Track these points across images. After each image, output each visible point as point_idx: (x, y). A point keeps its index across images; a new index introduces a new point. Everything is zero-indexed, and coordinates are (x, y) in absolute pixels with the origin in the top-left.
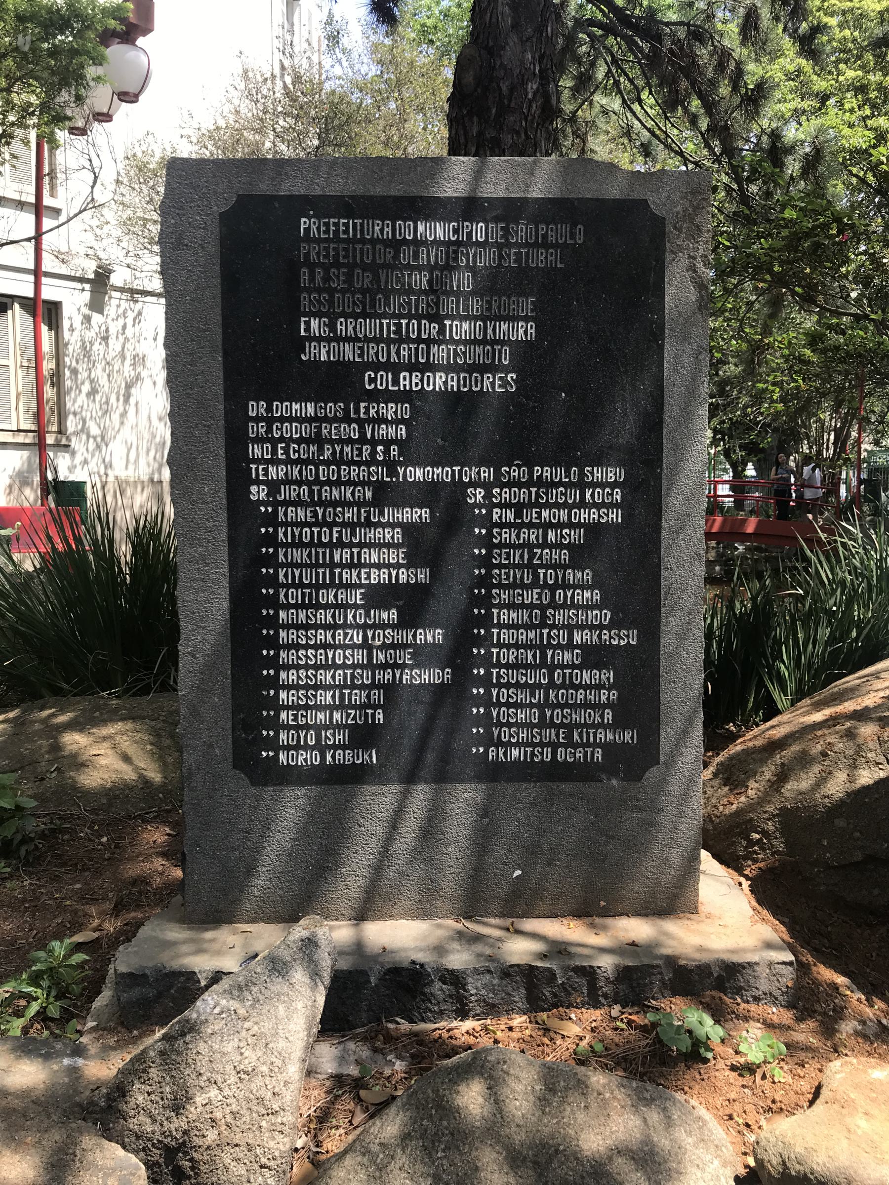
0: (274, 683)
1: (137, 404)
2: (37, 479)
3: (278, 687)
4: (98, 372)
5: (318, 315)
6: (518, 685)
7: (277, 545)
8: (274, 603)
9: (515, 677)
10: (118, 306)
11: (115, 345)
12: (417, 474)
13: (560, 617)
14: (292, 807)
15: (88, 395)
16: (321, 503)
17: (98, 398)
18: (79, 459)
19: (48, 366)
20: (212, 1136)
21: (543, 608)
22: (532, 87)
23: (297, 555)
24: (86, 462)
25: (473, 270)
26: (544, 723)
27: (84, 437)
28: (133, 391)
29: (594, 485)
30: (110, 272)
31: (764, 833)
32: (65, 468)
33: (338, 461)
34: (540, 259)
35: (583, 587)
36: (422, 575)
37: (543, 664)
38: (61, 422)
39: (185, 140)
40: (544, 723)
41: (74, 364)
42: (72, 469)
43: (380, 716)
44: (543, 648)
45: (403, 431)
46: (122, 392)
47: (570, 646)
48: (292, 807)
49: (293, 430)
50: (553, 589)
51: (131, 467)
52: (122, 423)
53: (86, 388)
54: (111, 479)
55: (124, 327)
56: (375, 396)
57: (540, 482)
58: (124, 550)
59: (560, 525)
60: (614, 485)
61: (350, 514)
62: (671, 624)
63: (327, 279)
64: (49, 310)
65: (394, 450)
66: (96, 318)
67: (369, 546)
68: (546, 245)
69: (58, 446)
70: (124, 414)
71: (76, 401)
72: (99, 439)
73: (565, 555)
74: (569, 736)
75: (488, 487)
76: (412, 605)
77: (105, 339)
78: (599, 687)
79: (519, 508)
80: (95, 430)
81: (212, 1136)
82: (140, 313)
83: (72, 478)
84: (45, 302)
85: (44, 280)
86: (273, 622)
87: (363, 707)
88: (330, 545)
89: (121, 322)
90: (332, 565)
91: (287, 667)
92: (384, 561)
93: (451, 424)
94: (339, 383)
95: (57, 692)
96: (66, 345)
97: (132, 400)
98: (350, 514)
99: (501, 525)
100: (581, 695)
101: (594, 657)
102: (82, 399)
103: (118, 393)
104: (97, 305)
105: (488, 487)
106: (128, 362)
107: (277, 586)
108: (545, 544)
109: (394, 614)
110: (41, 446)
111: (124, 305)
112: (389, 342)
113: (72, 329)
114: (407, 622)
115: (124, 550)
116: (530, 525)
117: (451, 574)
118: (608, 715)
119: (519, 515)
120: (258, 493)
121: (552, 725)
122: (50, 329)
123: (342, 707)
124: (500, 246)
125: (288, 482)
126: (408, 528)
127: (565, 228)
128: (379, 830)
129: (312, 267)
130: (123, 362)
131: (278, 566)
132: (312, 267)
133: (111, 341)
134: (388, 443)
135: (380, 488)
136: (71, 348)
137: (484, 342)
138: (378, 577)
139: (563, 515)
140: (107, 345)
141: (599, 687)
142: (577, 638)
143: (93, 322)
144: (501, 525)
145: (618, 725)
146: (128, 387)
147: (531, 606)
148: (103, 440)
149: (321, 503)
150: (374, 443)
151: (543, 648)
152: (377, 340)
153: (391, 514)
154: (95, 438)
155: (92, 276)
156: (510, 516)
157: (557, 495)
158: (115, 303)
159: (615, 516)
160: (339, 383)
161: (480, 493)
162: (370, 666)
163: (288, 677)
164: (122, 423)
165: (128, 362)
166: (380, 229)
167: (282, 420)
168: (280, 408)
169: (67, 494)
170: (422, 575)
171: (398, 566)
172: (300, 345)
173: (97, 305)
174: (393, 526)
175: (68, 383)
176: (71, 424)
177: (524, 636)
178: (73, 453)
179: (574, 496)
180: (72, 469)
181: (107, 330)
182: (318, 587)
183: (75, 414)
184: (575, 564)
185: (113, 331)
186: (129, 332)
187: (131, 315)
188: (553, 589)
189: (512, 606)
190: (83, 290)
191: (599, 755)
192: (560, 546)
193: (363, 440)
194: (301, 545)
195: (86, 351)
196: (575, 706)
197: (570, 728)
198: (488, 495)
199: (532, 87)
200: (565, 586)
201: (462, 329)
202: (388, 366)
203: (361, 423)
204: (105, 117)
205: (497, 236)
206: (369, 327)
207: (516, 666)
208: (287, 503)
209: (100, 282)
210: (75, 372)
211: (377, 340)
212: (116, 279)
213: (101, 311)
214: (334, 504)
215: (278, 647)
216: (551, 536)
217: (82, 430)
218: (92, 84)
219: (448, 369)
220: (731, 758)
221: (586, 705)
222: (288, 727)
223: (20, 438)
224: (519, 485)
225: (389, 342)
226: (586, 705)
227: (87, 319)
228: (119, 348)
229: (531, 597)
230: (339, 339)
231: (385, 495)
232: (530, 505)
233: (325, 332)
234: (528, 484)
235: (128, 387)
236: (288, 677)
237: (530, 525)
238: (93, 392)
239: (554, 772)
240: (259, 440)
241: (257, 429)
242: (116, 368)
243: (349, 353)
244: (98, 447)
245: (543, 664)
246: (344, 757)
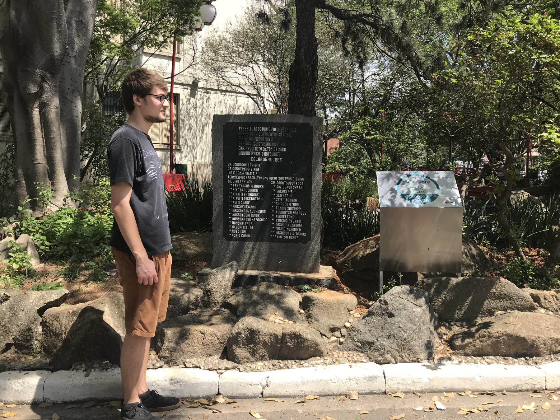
0: (231, 220)
1: (206, 134)
2: (169, 163)
3: (232, 221)
4: (192, 121)
5: (242, 146)
6: (281, 222)
7: (233, 192)
8: (232, 203)
9: (280, 221)
10: (201, 95)
11: (199, 110)
12: (261, 178)
13: (290, 209)
14: (233, 245)
15: (188, 130)
16: (242, 183)
17: (192, 131)
18: (184, 155)
19: (174, 118)
20: (214, 290)
21: (287, 207)
22: (309, 74)
23: (237, 194)
24: (186, 156)
25: (273, 137)
26: (286, 231)
27: (186, 146)
28: (205, 128)
29: (297, 181)
30: (198, 82)
31: (348, 264)
32: (179, 159)
33: (245, 175)
34: (286, 135)
35: (295, 202)
36: (262, 199)
37: (286, 218)
38: (178, 140)
39: (228, 33)
40: (286, 231)
41: (183, 118)
42: (181, 159)
43: (252, 228)
44: (287, 215)
45: (258, 169)
46: (201, 128)
47: (292, 215)
48: (233, 245)
49: (237, 169)
50: (289, 202)
51: (203, 159)
52: (200, 141)
53: (187, 127)
54: (195, 163)
55: (203, 103)
56: (253, 162)
57: (286, 180)
58: (201, 190)
59: (290, 189)
60: (302, 181)
61: (247, 186)
62: (313, 211)
63: (244, 139)
64: (175, 98)
65: (257, 173)
66: (192, 100)
67: (251, 192)
68: (288, 132)
69: (176, 150)
70: (201, 138)
71: (184, 132)
72: (192, 147)
73: (291, 196)
74: (292, 234)
75: (275, 181)
76: (259, 205)
77: (195, 108)
78: (298, 223)
79: (282, 186)
80: (190, 144)
81: (214, 290)
82: (209, 97)
83: (181, 163)
84: (174, 94)
85: (174, 86)
86: (231, 207)
87: (249, 226)
88: (243, 192)
89: (201, 101)
90: (243, 196)
91: (234, 217)
92: (253, 196)
93: (266, 169)
94: (246, 159)
95: (181, 231)
96: (181, 110)
97: (205, 132)
98: (247, 186)
99: (278, 189)
100: (294, 225)
101: (297, 217)
102: (186, 132)
103: (199, 129)
104: (193, 95)
105: (275, 181)
106: (204, 117)
107: (232, 200)
108: (287, 193)
109: (256, 207)
110: (171, 150)
111: (203, 94)
112: (256, 151)
113: (183, 104)
114: (258, 209)
115: (201, 190)
116: (284, 189)
117: (268, 199)
118: (300, 229)
119: (282, 187)
120: (229, 181)
121: (288, 231)
122: (175, 104)
123: (245, 225)
124: (279, 132)
125: (235, 179)
126: (259, 189)
127: (292, 129)
128: (250, 250)
129: (241, 136)
130: (202, 117)
131: (233, 196)
132: (241, 136)
133: (198, 109)
134: (255, 172)
135: (253, 180)
136: (182, 112)
137: (275, 152)
138: (253, 199)
139: (291, 187)
140: (196, 110)
141: (298, 223)
142: (294, 213)
143: (191, 102)
144: (278, 189)
145: (302, 232)
146: (203, 127)
147: (284, 206)
148: (193, 148)
149: (242, 183)
150: (252, 172)
151: (287, 215)
152: (254, 151)
153: (255, 186)
154: (190, 147)
155: (191, 83)
156: (280, 187)
157: (290, 183)
158: (199, 93)
159: (302, 188)
160: (246, 159)
161: (274, 182)
162: (251, 217)
163: (234, 219)
164: (200, 141)
165: (204, 117)
166: (255, 129)
167: (234, 167)
168: (234, 164)
169: (180, 169)
170: (262, 199)
171: (257, 197)
172: (238, 152)
173: (193, 95)
174: (256, 188)
175: (181, 125)
176: (182, 141)
177: (282, 212)
178: (182, 153)
179: (293, 183)
180: (181, 159)
181: (196, 104)
182: (240, 201)
183: (183, 137)
184: (293, 198)
185: (198, 104)
186: (204, 105)
187: (205, 98)
188: (289, 202)
189: (280, 206)
190: (188, 89)
191: (298, 238)
192: (290, 194)
193: (250, 171)
194: (238, 192)
195: (188, 114)
196: (293, 227)
197: (292, 232)
198: (276, 183)
199: (309, 74)
200: (291, 202)
201: (270, 149)
202: (256, 156)
203: (250, 167)
204: (200, 30)
205: (278, 130)
206: (252, 148)
207: (281, 218)
208: (235, 183)
209: (194, 86)
210: (183, 121)
211: (254, 151)
212: (200, 84)
213: (194, 97)
214: (244, 184)
215: (232, 213)
216: (289, 191)
217: (185, 144)
218: (195, 22)
219: (268, 157)
220: (34, 127)
221: (295, 227)
222: (234, 229)
223: (162, 147)
224: (282, 181)
225: (256, 151)
226: (295, 227)
227: (189, 100)
228: (200, 112)
229: (284, 204)
230: (246, 151)
231: (254, 182)
232: (284, 185)
233: (243, 149)
234: (284, 181)
235: (203, 127)
236: (234, 219)
237: (284, 189)
238: (190, 129)
239: (288, 241)
240: (230, 171)
241: (229, 168)
242: (199, 119)
243: (248, 154)
244: (191, 150)
245: (286, 218)
246: (245, 236)
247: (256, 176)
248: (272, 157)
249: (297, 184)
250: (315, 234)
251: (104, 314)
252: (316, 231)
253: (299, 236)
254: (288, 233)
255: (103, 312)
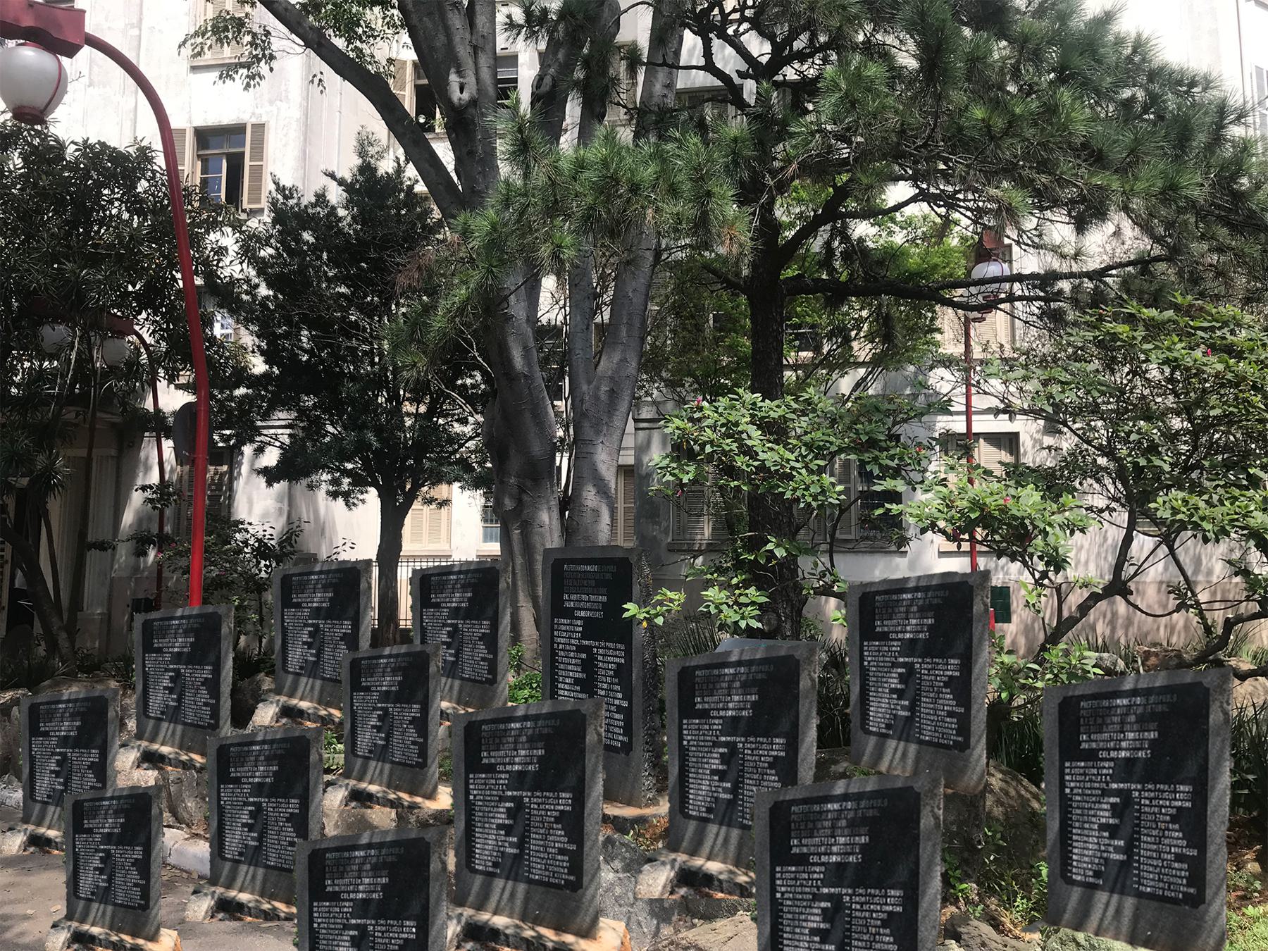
47: (1170, 853)
78: (1181, 870)
101: (951, 714)
138: (1104, 820)
141: (1181, 870)
189: (1148, 835)
197: (1170, 884)
205: (1144, 702)
241: (1067, 771)
247: (1107, 784)
248: (1134, 749)
249: (1181, 796)
250: (978, 741)
251: (87, 16)
252: (980, 737)
253: (1184, 893)
254: (1161, 885)
255: (84, 12)
